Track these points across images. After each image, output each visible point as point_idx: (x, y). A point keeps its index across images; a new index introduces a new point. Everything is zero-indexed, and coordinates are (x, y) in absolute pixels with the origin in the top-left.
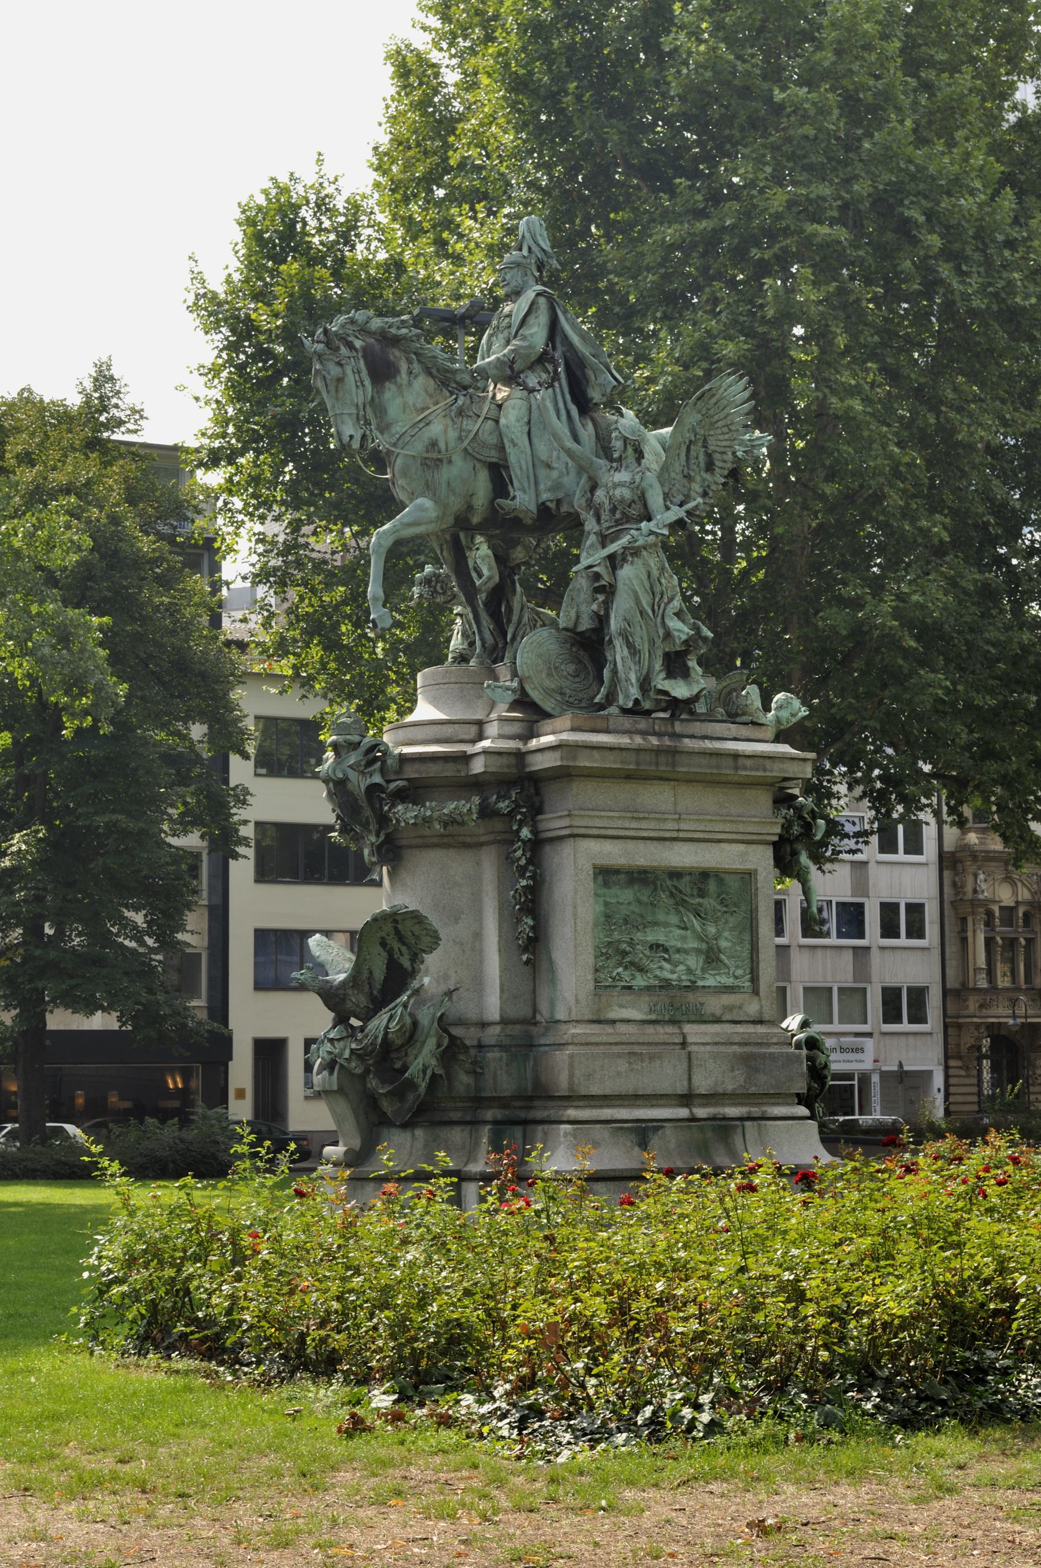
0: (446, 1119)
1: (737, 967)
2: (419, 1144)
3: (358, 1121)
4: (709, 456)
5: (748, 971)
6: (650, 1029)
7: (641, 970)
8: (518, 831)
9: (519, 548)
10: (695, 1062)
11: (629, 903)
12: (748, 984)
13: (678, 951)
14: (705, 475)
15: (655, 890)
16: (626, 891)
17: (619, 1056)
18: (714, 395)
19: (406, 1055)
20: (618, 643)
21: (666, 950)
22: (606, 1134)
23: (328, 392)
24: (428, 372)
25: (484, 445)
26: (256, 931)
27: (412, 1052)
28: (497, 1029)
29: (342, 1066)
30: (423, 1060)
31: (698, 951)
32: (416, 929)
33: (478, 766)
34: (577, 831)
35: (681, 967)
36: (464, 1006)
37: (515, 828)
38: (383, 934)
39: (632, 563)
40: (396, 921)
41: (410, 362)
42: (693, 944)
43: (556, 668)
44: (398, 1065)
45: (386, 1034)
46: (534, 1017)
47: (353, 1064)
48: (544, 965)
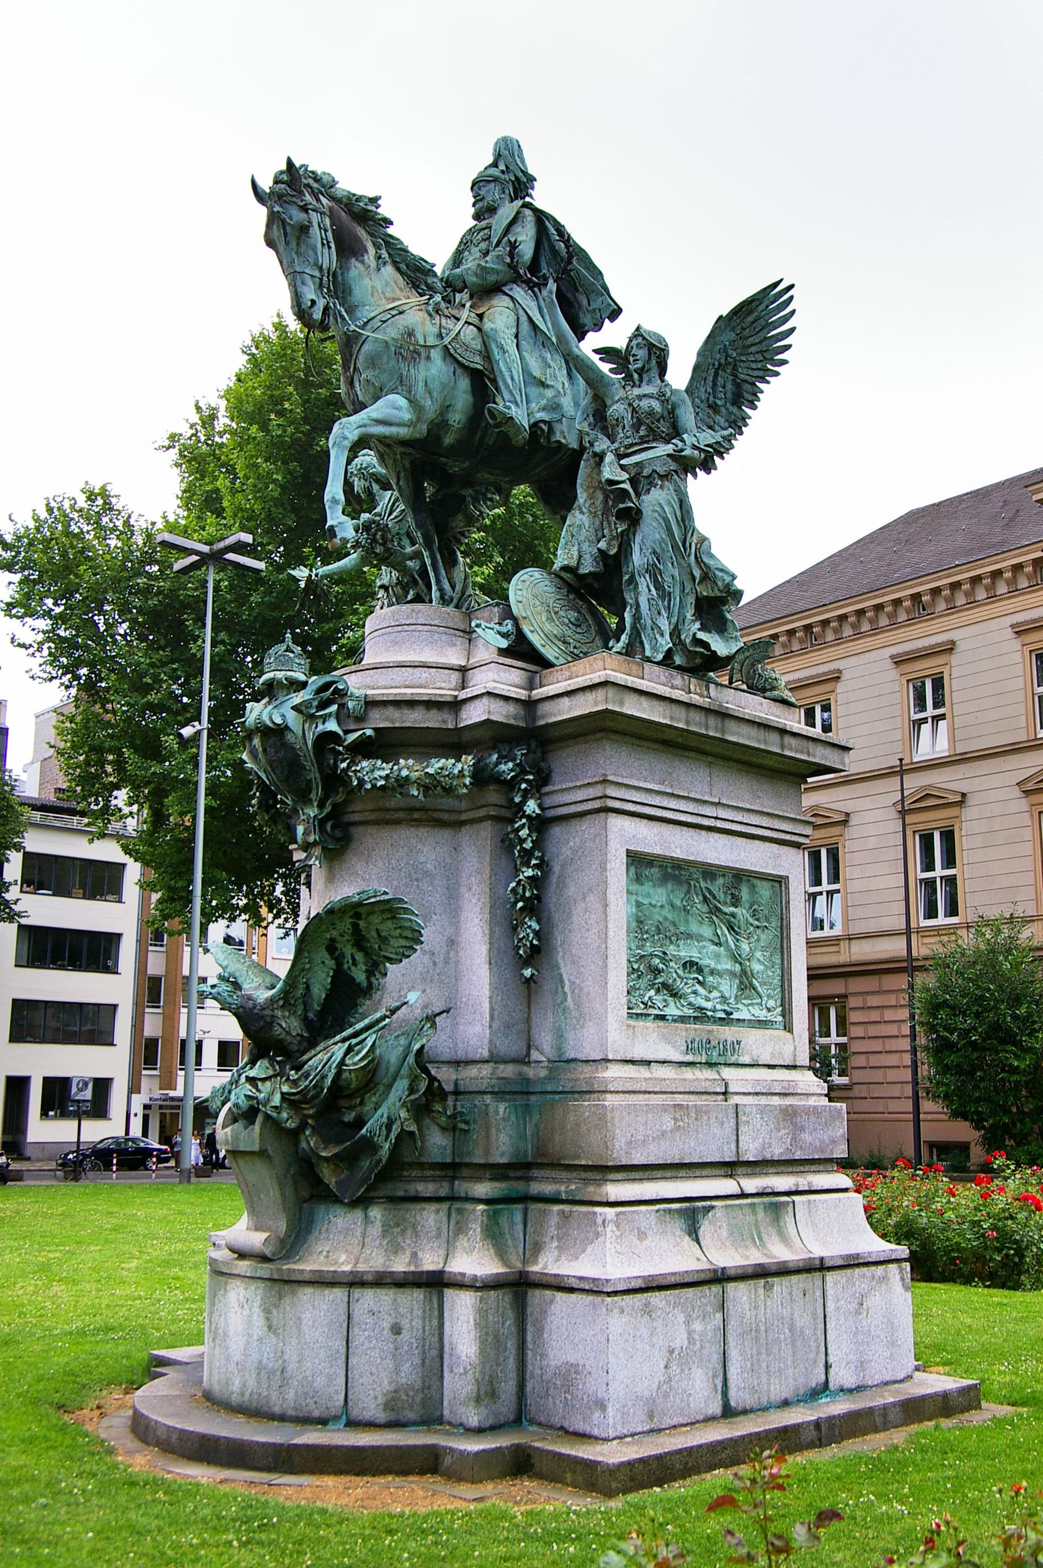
0: (412, 1193)
1: (769, 997)
2: (375, 1230)
3: (283, 1194)
4: (737, 386)
5: (779, 1003)
6: (689, 1074)
7: (675, 995)
8: (524, 802)
9: (460, 517)
10: (743, 1118)
11: (662, 906)
12: (780, 1018)
13: (712, 972)
14: (731, 408)
15: (688, 892)
16: (659, 890)
17: (664, 1109)
18: (751, 312)
19: (362, 1103)
20: (644, 583)
21: (700, 970)
22: (653, 1219)
23: (287, 243)
24: (396, 265)
25: (466, 347)
26: (14, 1001)
27: (371, 1100)
28: (486, 1070)
29: (267, 1117)
30: (387, 1111)
31: (732, 974)
32: (387, 928)
33: (474, 714)
34: (611, 804)
35: (715, 994)
36: (439, 1042)
37: (517, 800)
38: (334, 933)
39: (662, 487)
40: (358, 916)
41: (377, 247)
42: (727, 965)
43: (556, 613)
44: (349, 1117)
45: (339, 1072)
46: (528, 1054)
47: (285, 1115)
48: (548, 985)
